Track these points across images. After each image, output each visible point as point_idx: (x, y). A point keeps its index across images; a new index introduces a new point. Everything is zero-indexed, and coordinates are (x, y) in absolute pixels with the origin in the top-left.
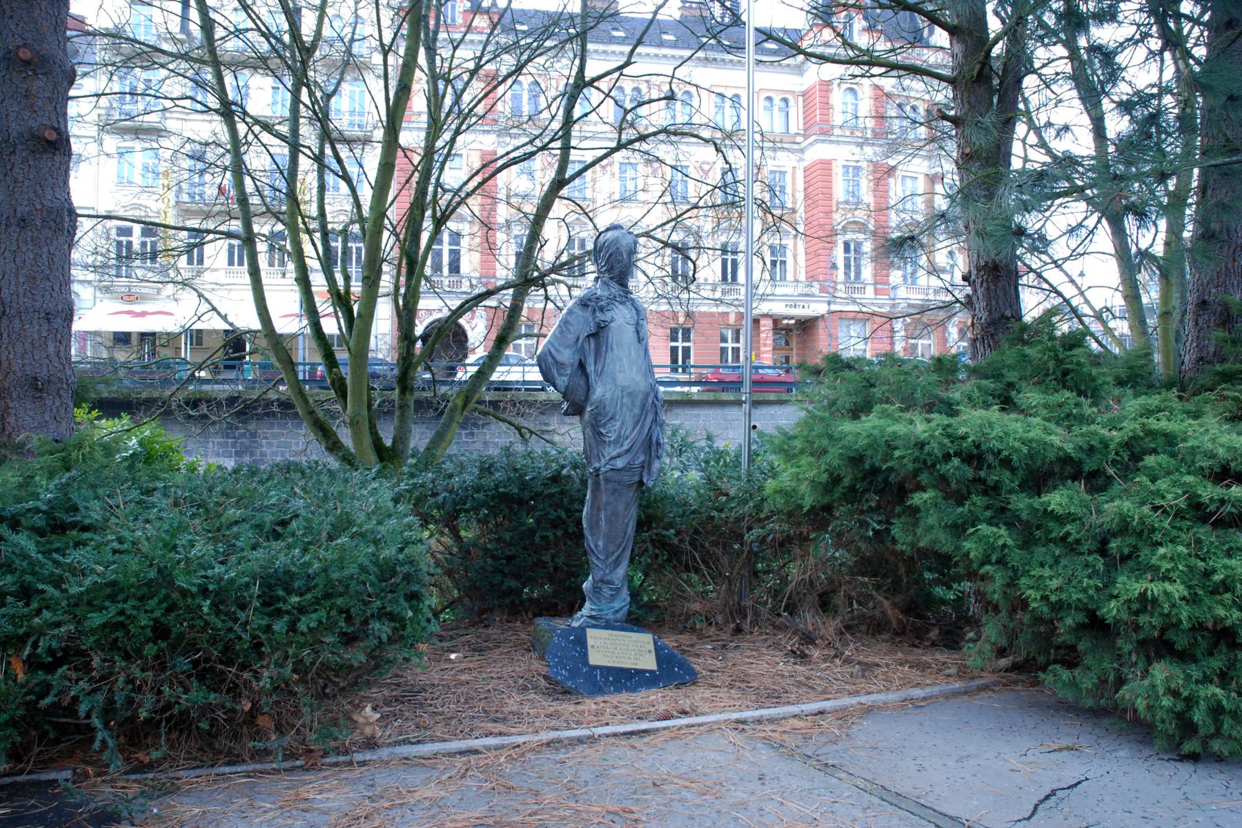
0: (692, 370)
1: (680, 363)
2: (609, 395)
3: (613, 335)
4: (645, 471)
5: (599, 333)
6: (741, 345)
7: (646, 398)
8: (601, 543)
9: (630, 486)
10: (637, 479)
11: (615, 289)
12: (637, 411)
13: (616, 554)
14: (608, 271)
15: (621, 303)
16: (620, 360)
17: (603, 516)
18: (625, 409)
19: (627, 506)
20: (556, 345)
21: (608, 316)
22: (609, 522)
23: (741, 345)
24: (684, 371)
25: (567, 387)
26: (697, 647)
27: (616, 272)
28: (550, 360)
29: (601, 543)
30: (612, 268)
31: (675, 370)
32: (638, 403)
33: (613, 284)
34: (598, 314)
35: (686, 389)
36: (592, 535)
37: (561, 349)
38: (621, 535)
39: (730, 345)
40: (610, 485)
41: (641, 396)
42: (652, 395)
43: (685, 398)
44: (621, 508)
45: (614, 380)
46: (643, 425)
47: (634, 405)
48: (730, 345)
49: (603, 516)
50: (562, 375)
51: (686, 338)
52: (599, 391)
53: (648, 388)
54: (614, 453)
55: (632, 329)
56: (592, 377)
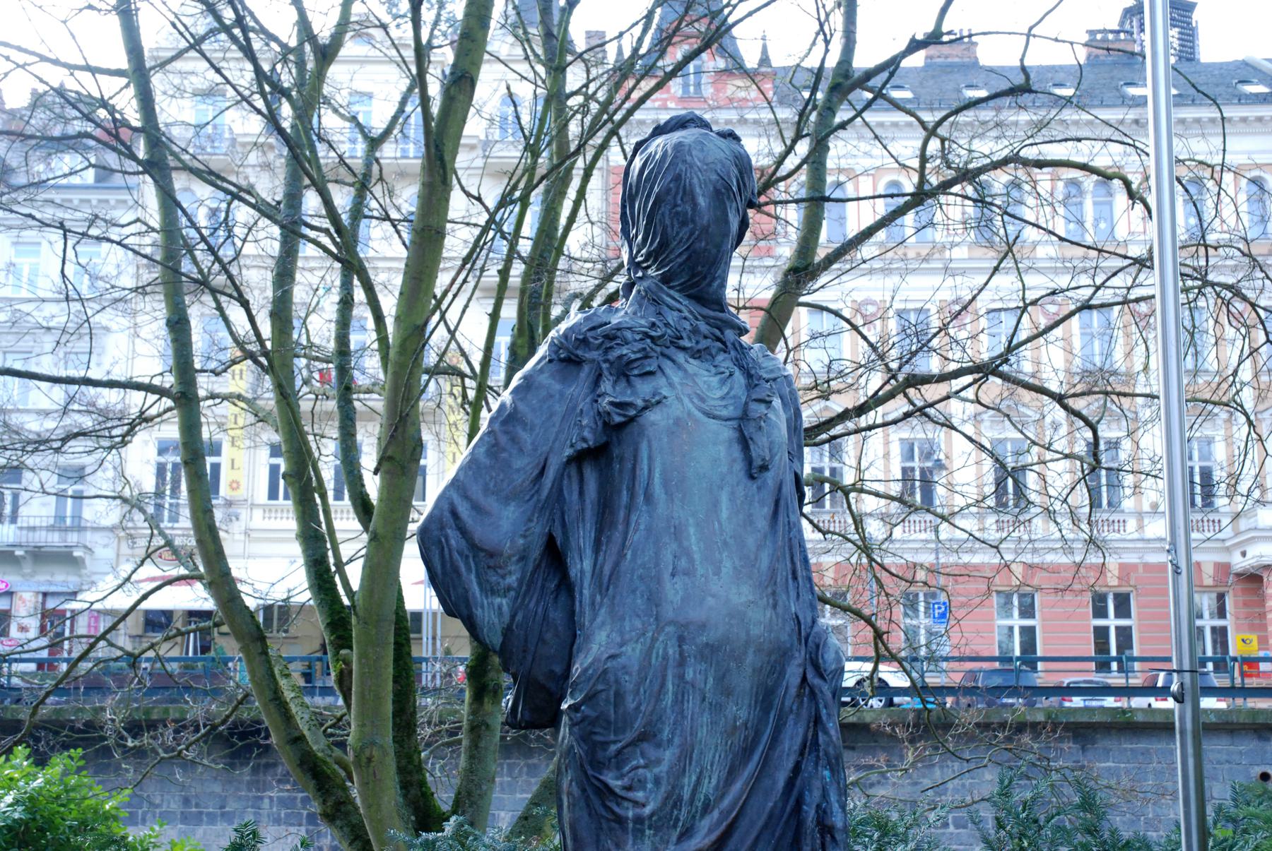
0: (1137, 665)
1: (1114, 653)
2: (633, 653)
5: (607, 449)
6: (1228, 622)
11: (680, 312)
12: (740, 711)
14: (653, 256)
15: (697, 354)
16: (678, 533)
18: (691, 705)
20: (476, 491)
23: (1228, 622)
24: (1120, 670)
25: (507, 632)
27: (678, 254)
30: (664, 245)
31: (1103, 666)
32: (744, 681)
33: (672, 297)
34: (606, 386)
35: (1122, 703)
37: (491, 503)
39: (1207, 623)
42: (799, 657)
43: (1120, 719)
45: (654, 600)
47: (728, 692)
48: (1207, 623)
50: (491, 591)
51: (1123, 606)
52: (598, 644)
53: (785, 635)
55: (726, 432)
56: (586, 591)
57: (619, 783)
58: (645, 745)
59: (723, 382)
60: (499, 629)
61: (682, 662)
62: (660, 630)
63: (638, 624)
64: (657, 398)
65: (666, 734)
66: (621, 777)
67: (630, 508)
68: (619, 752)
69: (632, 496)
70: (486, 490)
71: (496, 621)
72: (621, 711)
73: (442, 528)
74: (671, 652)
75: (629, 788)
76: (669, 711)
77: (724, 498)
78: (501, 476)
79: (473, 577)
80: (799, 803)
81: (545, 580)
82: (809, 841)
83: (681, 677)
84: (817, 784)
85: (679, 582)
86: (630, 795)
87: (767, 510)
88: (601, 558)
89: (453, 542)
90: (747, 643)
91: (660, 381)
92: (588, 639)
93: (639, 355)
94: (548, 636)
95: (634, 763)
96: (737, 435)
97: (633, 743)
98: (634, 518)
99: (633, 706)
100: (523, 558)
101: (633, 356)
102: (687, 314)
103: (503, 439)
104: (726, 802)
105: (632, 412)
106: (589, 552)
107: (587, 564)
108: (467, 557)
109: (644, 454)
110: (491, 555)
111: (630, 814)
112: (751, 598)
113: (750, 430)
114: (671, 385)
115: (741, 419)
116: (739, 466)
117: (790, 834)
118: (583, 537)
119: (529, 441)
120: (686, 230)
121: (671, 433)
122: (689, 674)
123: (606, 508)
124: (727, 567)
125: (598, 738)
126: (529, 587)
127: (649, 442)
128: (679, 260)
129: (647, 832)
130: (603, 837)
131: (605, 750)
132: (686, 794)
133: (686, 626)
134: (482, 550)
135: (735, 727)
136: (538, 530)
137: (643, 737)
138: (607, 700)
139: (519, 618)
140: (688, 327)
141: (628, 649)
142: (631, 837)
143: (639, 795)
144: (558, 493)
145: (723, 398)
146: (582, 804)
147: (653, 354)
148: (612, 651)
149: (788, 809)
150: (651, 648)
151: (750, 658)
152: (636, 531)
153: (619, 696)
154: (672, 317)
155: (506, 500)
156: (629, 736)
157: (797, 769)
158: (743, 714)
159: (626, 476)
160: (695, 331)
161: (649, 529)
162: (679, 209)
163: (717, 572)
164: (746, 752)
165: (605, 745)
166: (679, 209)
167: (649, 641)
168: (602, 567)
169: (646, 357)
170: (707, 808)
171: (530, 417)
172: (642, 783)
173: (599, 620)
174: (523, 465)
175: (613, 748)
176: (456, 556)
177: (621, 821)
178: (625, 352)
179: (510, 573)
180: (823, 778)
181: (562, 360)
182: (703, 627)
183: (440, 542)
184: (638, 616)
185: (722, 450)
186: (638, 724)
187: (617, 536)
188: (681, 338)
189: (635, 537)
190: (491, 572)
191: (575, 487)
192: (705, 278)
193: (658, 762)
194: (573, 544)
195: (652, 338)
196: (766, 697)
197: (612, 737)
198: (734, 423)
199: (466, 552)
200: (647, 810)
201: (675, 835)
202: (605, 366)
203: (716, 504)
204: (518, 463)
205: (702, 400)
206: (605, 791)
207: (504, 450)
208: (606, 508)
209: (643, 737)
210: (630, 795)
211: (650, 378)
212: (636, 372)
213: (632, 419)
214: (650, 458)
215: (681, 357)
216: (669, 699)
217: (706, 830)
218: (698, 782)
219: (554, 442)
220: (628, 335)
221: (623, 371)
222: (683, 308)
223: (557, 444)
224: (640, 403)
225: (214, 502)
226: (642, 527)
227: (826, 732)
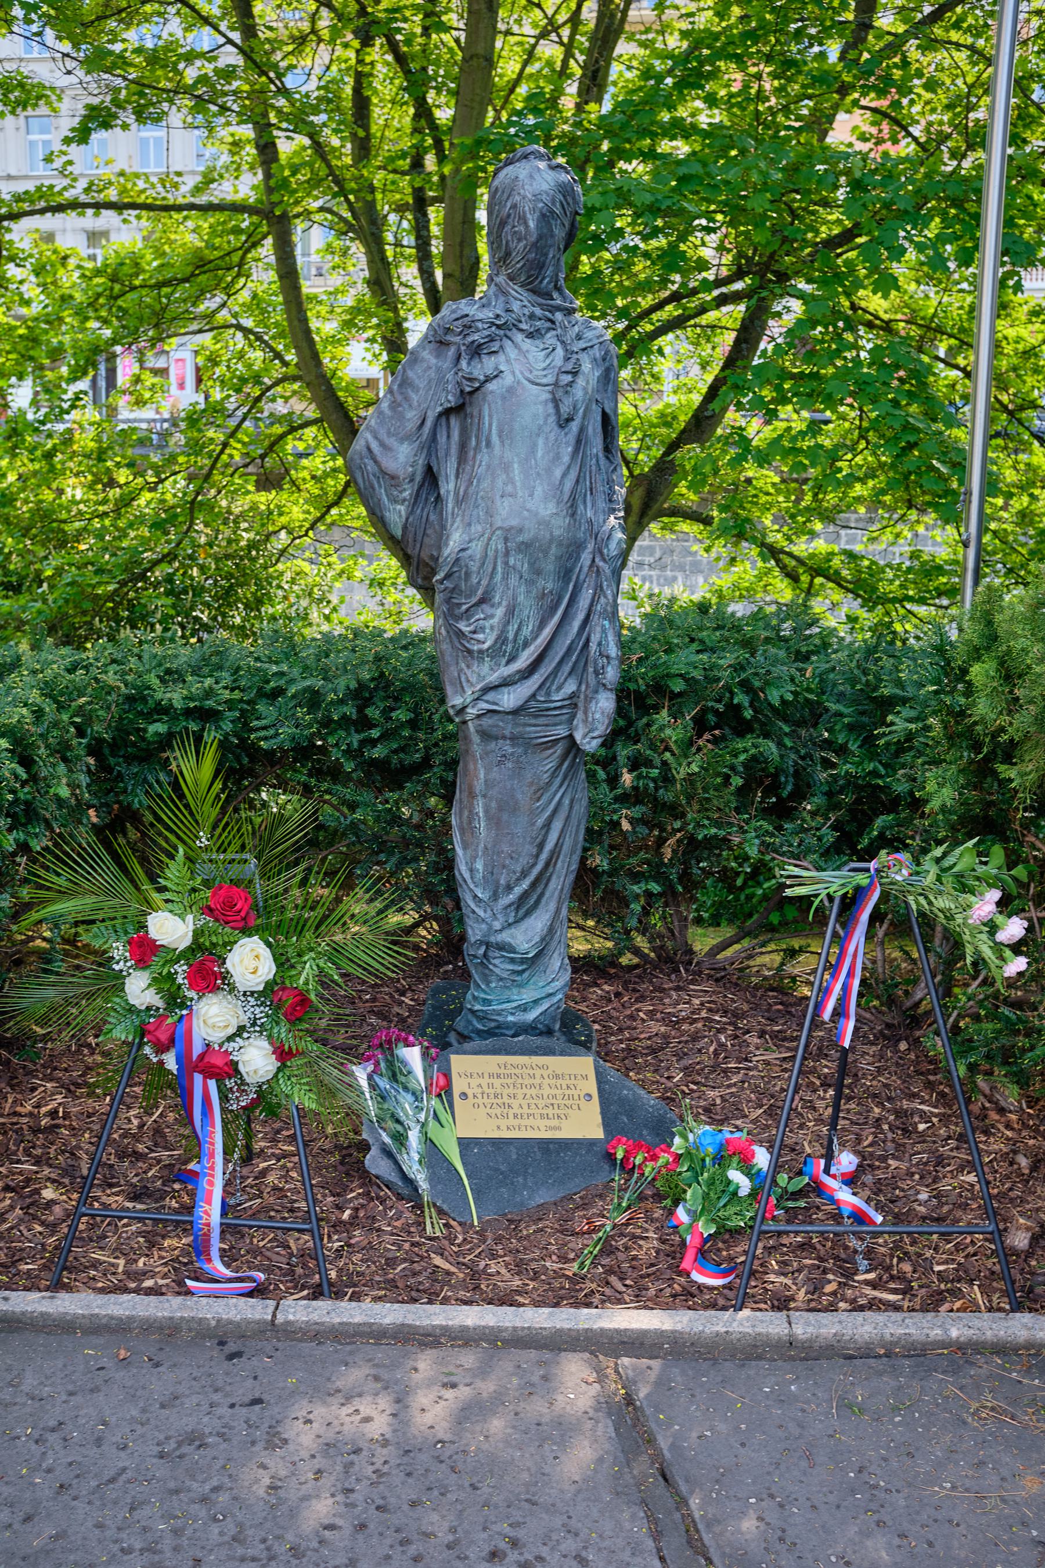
2: (476, 549)
3: (490, 414)
4: (580, 715)
8: (479, 865)
13: (518, 890)
15: (530, 335)
16: (507, 468)
17: (480, 810)
18: (513, 581)
21: (480, 369)
25: (405, 528)
26: (72, 1475)
28: (371, 467)
29: (479, 865)
32: (549, 566)
33: (515, 290)
34: (464, 364)
37: (392, 442)
45: (489, 514)
47: (538, 572)
49: (480, 810)
50: (395, 501)
54: (494, 678)
60: (400, 526)
61: (507, 554)
63: (479, 528)
65: (497, 599)
70: (389, 433)
77: (541, 442)
83: (506, 563)
85: (507, 502)
90: (551, 542)
91: (501, 358)
103: (399, 398)
106: (453, 478)
109: (486, 413)
110: (393, 477)
114: (508, 361)
116: (552, 419)
118: (448, 468)
121: (504, 398)
122: (512, 562)
124: (539, 491)
132: (511, 636)
133: (509, 530)
137: (482, 601)
141: (473, 544)
143: (481, 636)
151: (554, 550)
155: (402, 440)
161: (488, 466)
163: (531, 495)
165: (460, 605)
170: (526, 644)
172: (482, 629)
174: (412, 416)
182: (520, 531)
185: (541, 408)
193: (492, 616)
200: (486, 646)
201: (504, 661)
203: (534, 446)
204: (410, 415)
206: (460, 634)
209: (482, 601)
216: (499, 577)
218: (519, 629)
220: (480, 325)
221: (476, 351)
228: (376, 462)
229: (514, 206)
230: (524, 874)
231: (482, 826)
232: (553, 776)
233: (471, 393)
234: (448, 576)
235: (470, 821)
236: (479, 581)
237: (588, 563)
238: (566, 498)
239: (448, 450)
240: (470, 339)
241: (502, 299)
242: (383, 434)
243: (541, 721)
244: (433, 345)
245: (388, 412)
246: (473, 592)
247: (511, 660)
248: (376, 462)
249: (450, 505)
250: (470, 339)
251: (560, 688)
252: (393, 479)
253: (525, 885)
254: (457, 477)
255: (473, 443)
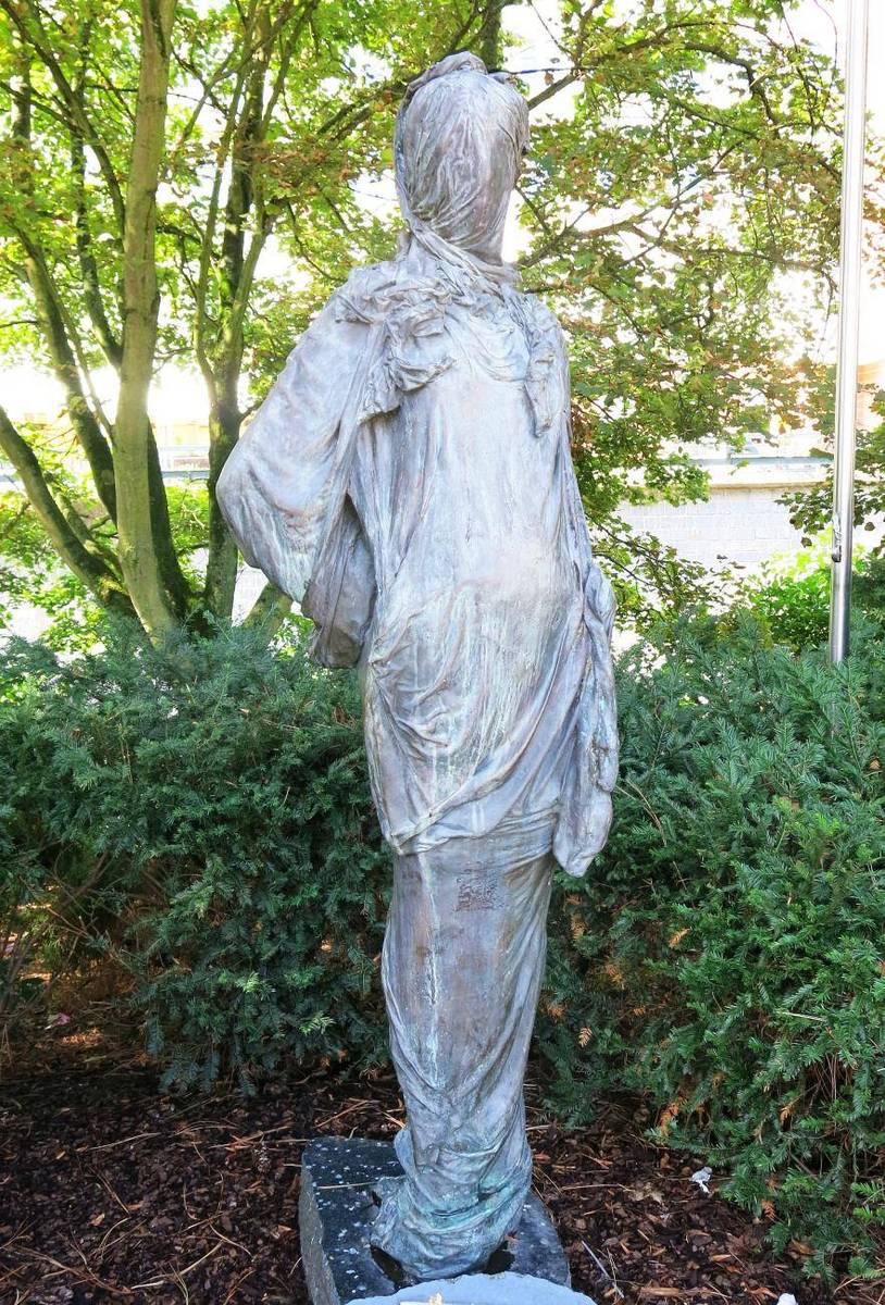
7: (559, 616)
8: (433, 1045)
9: (516, 874)
10: (539, 851)
12: (528, 656)
13: (482, 1069)
15: (480, 312)
18: (487, 657)
19: (510, 932)
21: (426, 356)
22: (452, 981)
28: (255, 500)
29: (433, 1045)
32: (532, 631)
34: (397, 349)
36: (409, 1021)
37: (286, 464)
38: (494, 1014)
40: (453, 883)
41: (540, 610)
42: (578, 602)
44: (491, 944)
45: (451, 562)
46: (550, 698)
47: (518, 641)
54: (459, 792)
55: (513, 393)
56: (386, 552)
57: (424, 727)
58: (446, 693)
59: (505, 340)
61: (478, 620)
62: (457, 590)
63: (437, 584)
64: (448, 363)
66: (426, 722)
67: (424, 473)
68: (423, 701)
69: (426, 461)
70: (282, 451)
71: (298, 575)
72: (424, 664)
73: (241, 488)
74: (468, 611)
75: (433, 732)
76: (467, 662)
78: (296, 439)
79: (274, 533)
80: (577, 730)
81: (343, 536)
82: (586, 761)
83: (478, 631)
84: (593, 713)
86: (435, 737)
87: (549, 467)
88: (397, 521)
89: (252, 501)
92: (388, 599)
93: (426, 317)
94: (348, 589)
95: (437, 709)
96: (521, 395)
97: (436, 692)
98: (429, 482)
99: (435, 659)
100: (322, 518)
101: (421, 318)
102: (466, 269)
103: (295, 401)
104: (515, 736)
105: (424, 379)
107: (385, 524)
108: (267, 515)
111: (434, 753)
112: (539, 555)
113: (534, 390)
115: (525, 379)
116: (525, 426)
117: (569, 754)
119: (322, 404)
120: (467, 184)
123: (400, 470)
125: (402, 689)
126: (329, 546)
127: (441, 407)
128: (461, 216)
129: (450, 768)
130: (410, 772)
131: (410, 699)
132: (483, 736)
133: (481, 585)
134: (280, 509)
135: (525, 671)
136: (335, 492)
137: (444, 687)
138: (411, 656)
139: (321, 574)
140: (469, 283)
142: (435, 772)
143: (442, 737)
144: (353, 456)
145: (505, 359)
146: (390, 744)
147: (439, 315)
148: (414, 612)
149: (568, 734)
150: (450, 606)
152: (431, 495)
153: (422, 651)
154: (453, 273)
156: (431, 687)
157: (575, 702)
158: (531, 659)
159: (420, 440)
160: (474, 287)
162: (461, 162)
164: (534, 690)
165: (410, 695)
166: (461, 162)
167: (448, 601)
168: (399, 530)
169: (433, 318)
170: (499, 741)
171: (321, 378)
173: (400, 579)
174: (319, 428)
175: (418, 698)
176: (257, 516)
177: (424, 759)
178: (413, 314)
179: (310, 531)
180: (599, 707)
181: (349, 321)
183: (240, 501)
184: (437, 577)
186: (440, 675)
187: (413, 499)
188: (462, 295)
189: (432, 501)
190: (291, 530)
191: (369, 449)
192: (485, 233)
193: (458, 707)
194: (370, 505)
195: (437, 297)
196: (551, 639)
197: (416, 688)
198: (519, 384)
199: (266, 511)
200: (449, 750)
201: (473, 768)
202: (394, 328)
204: (312, 425)
205: (488, 362)
207: (297, 412)
208: (400, 470)
209: (444, 687)
210: (435, 737)
211: (437, 340)
212: (423, 333)
213: (424, 386)
214: (443, 423)
215: (463, 314)
216: (466, 652)
217: (499, 761)
219: (346, 405)
220: (415, 295)
221: (412, 333)
222: (463, 264)
223: (349, 408)
224: (432, 370)
225: (169, 90)
226: (437, 491)
227: (603, 669)
228: (263, 493)
229: (459, 130)
230: (490, 1047)
231: (436, 990)
232: (525, 910)
233: (414, 392)
234: (395, 654)
235: (421, 984)
236: (440, 658)
237: (576, 623)
238: (550, 534)
239: (376, 472)
240: (405, 315)
241: (431, 264)
242: (272, 452)
243: (516, 840)
244: (344, 326)
245: (280, 423)
246: (429, 675)
247: (484, 765)
248: (263, 493)
249: (386, 552)
250: (405, 315)
251: (539, 795)
252: (288, 517)
253: (494, 1055)
254: (394, 511)
255: (419, 462)
